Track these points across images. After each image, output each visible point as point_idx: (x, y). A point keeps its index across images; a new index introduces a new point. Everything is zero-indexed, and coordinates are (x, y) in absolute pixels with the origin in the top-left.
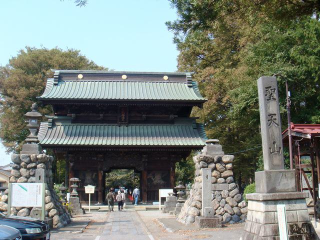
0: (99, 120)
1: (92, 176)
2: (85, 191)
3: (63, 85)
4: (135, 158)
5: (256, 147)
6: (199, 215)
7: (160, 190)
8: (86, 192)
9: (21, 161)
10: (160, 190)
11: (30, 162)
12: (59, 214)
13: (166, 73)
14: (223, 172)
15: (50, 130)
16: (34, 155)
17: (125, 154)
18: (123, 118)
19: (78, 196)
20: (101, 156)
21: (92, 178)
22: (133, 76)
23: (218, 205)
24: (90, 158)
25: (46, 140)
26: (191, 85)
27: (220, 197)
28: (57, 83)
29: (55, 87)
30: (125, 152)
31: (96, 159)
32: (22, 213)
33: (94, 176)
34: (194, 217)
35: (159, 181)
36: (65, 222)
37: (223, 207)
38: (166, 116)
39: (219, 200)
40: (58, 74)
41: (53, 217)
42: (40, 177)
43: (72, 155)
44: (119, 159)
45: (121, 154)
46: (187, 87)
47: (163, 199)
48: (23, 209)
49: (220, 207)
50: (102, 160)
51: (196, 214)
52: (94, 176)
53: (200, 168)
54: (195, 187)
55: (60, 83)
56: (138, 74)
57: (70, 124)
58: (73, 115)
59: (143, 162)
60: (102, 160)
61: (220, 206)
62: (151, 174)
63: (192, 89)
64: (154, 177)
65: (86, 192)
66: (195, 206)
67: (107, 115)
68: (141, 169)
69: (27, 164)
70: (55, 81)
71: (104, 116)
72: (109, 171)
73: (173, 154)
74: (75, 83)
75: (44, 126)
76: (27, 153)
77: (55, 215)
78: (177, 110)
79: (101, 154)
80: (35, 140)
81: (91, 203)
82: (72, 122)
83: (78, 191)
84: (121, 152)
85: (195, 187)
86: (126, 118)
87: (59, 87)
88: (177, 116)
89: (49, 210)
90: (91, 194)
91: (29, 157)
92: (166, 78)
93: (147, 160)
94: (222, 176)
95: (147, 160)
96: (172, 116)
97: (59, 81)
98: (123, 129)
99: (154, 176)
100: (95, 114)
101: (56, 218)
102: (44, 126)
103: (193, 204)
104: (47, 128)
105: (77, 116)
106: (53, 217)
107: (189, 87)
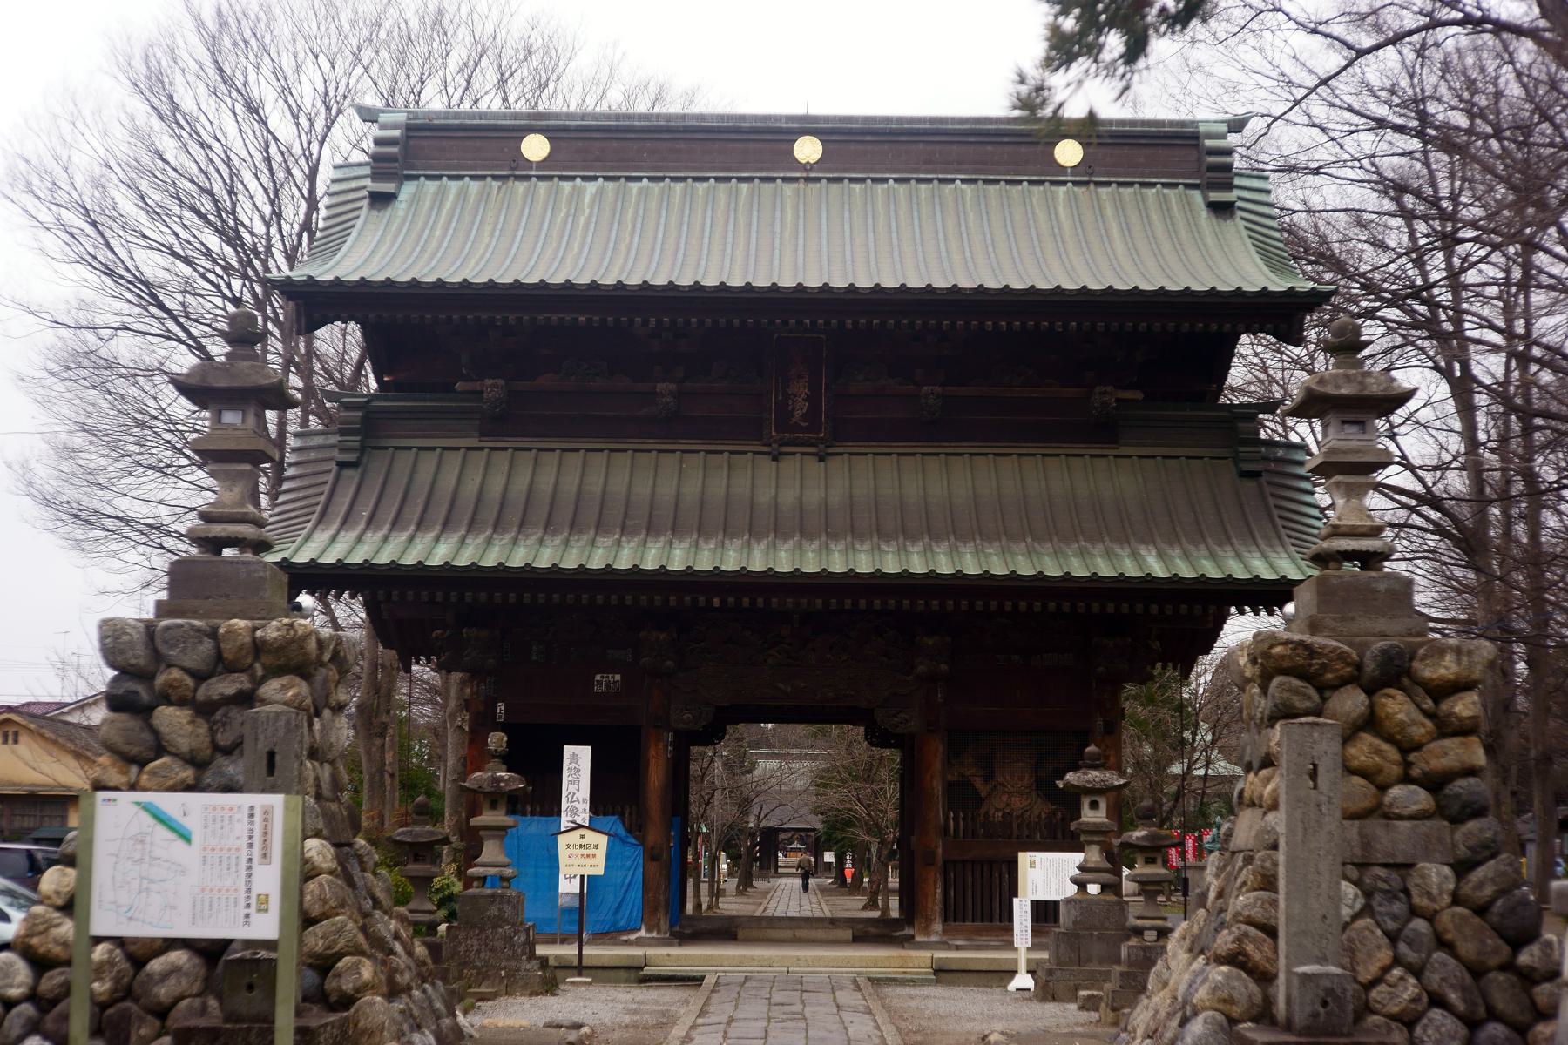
7: (1024, 858)
10: (1024, 858)
11: (222, 664)
18: (801, 407)
20: (662, 636)
40: (397, 133)
42: (271, 755)
57: (474, 442)
58: (493, 388)
69: (200, 677)
72: (712, 735)
82: (484, 434)
86: (814, 400)
95: (944, 667)
96: (1106, 396)
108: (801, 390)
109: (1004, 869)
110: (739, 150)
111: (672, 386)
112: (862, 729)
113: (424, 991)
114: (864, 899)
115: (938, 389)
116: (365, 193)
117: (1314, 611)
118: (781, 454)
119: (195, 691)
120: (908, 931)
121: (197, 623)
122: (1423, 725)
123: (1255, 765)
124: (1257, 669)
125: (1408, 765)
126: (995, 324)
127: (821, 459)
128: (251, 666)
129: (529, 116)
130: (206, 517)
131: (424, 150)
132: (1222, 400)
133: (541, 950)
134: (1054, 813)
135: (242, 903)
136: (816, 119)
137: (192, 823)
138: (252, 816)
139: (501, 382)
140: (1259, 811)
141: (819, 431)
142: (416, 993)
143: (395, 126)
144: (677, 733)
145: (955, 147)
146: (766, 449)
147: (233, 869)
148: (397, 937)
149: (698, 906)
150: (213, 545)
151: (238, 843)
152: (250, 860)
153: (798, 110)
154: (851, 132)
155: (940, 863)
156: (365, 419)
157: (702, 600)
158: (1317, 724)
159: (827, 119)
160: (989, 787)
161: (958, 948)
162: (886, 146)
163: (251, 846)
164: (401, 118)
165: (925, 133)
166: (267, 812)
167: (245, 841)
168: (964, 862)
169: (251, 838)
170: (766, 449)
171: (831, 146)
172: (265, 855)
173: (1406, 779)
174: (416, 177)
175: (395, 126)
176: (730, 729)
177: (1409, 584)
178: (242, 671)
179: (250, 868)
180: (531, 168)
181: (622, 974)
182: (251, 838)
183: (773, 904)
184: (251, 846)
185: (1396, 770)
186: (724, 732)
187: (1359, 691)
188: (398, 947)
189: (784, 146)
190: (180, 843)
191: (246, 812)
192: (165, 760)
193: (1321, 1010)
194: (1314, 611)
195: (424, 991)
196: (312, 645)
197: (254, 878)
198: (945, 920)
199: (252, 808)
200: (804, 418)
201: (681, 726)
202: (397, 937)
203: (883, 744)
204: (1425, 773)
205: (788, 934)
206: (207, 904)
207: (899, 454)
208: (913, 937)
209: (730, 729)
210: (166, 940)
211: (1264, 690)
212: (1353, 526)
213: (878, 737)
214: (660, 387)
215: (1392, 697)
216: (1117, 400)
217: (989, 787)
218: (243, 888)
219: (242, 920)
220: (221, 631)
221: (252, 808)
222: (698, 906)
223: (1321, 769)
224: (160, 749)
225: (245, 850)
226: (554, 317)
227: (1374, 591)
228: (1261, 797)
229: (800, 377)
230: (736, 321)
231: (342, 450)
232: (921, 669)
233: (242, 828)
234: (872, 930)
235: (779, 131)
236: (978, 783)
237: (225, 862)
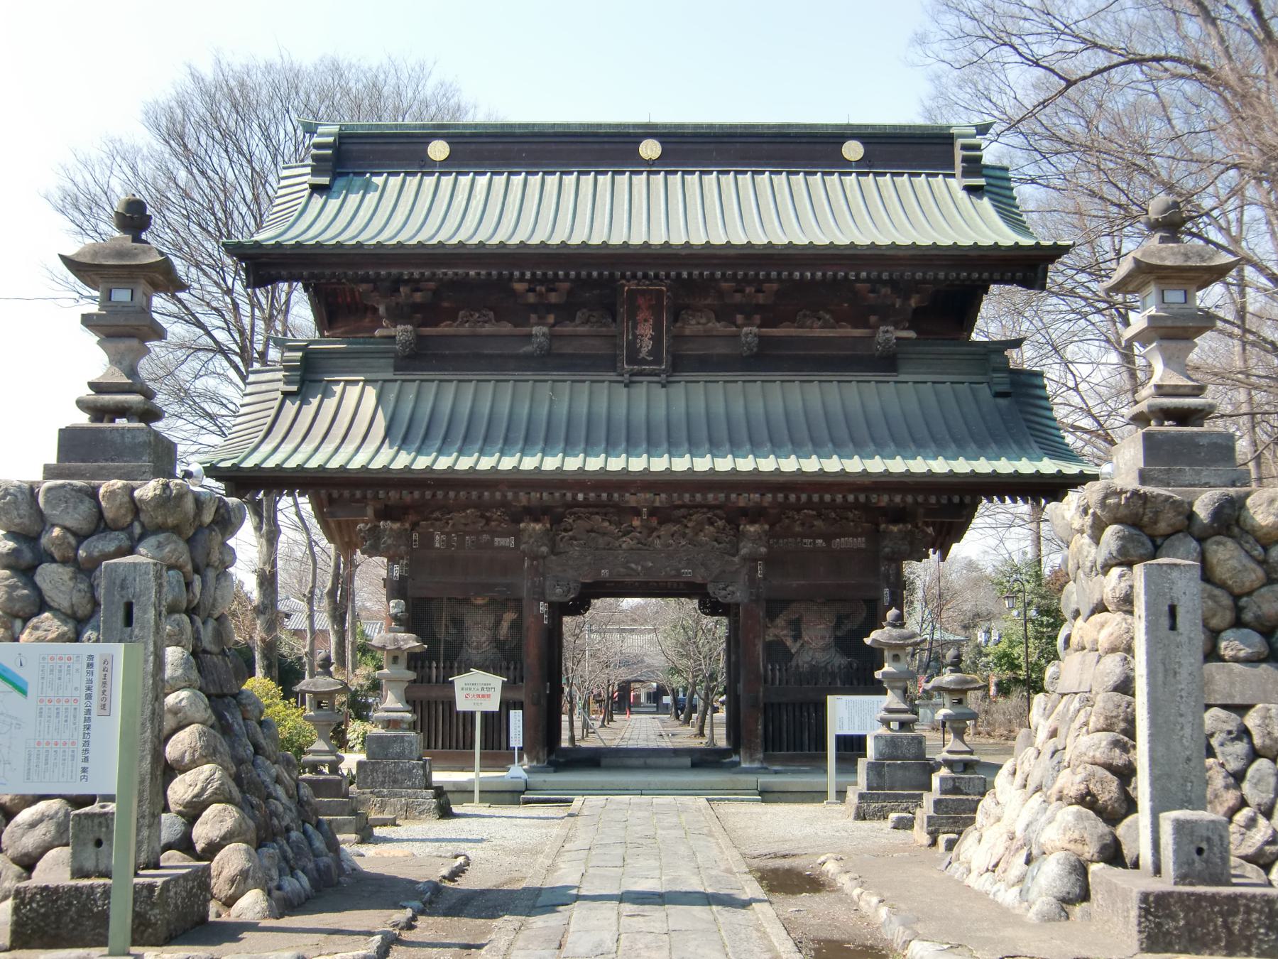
0: (528, 357)
1: (498, 623)
2: (452, 703)
3: (354, 199)
4: (702, 538)
5: (181, 881)
6: (1113, 855)
7: (829, 697)
8: (462, 705)
9: (43, 521)
10: (829, 697)
11: (100, 525)
12: (262, 834)
13: (849, 126)
14: (1249, 594)
15: (291, 408)
16: (118, 483)
17: (654, 522)
18: (646, 346)
19: (413, 726)
20: (538, 527)
21: (494, 639)
22: (696, 148)
23: (1230, 798)
24: (485, 537)
25: (266, 448)
26: (981, 182)
27: (1241, 747)
28: (325, 180)
29: (318, 201)
30: (653, 512)
31: (511, 542)
32: (33, 825)
33: (505, 626)
34: (1080, 870)
35: (822, 657)
36: (299, 883)
37: (1268, 814)
38: (858, 332)
39: (1233, 765)
40: (331, 139)
41: (212, 849)
42: (129, 607)
43: (396, 526)
44: (627, 542)
45: (636, 523)
46: (962, 195)
47: (852, 746)
48: (42, 806)
49: (1246, 812)
50: (544, 549)
51: (1090, 850)
52: (505, 626)
53: (1106, 568)
54: (1066, 683)
55: (341, 182)
56: (715, 135)
57: (390, 376)
58: (402, 331)
59: (744, 559)
60: (544, 549)
61: (1243, 803)
62: (780, 621)
63: (986, 202)
64: (797, 637)
65: (462, 705)
66: (1087, 800)
67: (568, 329)
68: (738, 593)
69: (81, 537)
70: (315, 172)
71: (552, 337)
72: (579, 606)
73: (895, 521)
74: (413, 182)
75: (264, 387)
76: (81, 476)
77: (227, 839)
78: (913, 303)
79: (537, 520)
80: (135, 398)
81: (483, 757)
82: (397, 369)
83: (412, 702)
84: (636, 512)
85: (1066, 683)
86: (657, 340)
87: (334, 204)
88: (912, 334)
89: (192, 812)
90: (485, 715)
91: (93, 493)
92: (853, 150)
93: (763, 550)
94: (1248, 616)
95: (763, 550)
96: (889, 334)
97: (335, 176)
98: (649, 400)
99: (796, 628)
100: (506, 328)
101: (232, 859)
102: (264, 387)
103: (1071, 782)
104: (280, 397)
105: (420, 338)
106: (212, 849)
107: (970, 190)
108: (646, 330)
109: (812, 709)
110: (600, 149)
111: (545, 329)
112: (696, 601)
113: (305, 832)
114: (695, 730)
115: (755, 329)
116: (306, 186)
117: (1141, 465)
118: (632, 382)
119: (77, 549)
120: (735, 758)
121: (78, 483)
122: (1254, 571)
123: (1085, 611)
124: (1088, 520)
125: (1238, 610)
126: (801, 275)
127: (664, 386)
128: (131, 524)
129: (435, 127)
130: (97, 387)
131: (351, 157)
132: (975, 337)
133: (438, 777)
134: (850, 664)
135: (80, 756)
136: (655, 126)
137: (28, 675)
138: (90, 665)
139: (409, 327)
140: (1094, 655)
141: (661, 364)
142: (295, 835)
143: (329, 135)
144: (551, 605)
145: (765, 146)
146: (620, 378)
147: (71, 719)
148: (278, 780)
149: (572, 738)
150: (98, 412)
151: (76, 694)
152: (88, 712)
153: (643, 119)
154: (683, 135)
155: (762, 705)
156: (304, 359)
157: (569, 495)
158: (1175, 565)
159: (665, 126)
160: (798, 645)
161: (776, 772)
162: (712, 146)
163: (89, 697)
164: (335, 129)
165: (741, 135)
166: (107, 664)
167: (84, 692)
168: (780, 704)
169: (89, 688)
170: (620, 378)
171: (669, 146)
172: (103, 707)
173: (1238, 623)
174: (347, 174)
175: (329, 135)
176: (594, 601)
177: (1231, 438)
178: (122, 529)
179: (87, 720)
180: (435, 166)
181: (507, 796)
182: (89, 688)
183: (304, 323)
184: (89, 697)
185: (1229, 616)
186: (589, 604)
187: (1190, 539)
188: (280, 791)
189: (632, 146)
190: (16, 695)
191: (85, 661)
192: (47, 614)
193: (1196, 857)
194: (1141, 465)
195: (305, 832)
196: (189, 504)
197: (92, 731)
198: (766, 750)
199: (91, 657)
200: (649, 353)
201: (554, 599)
202: (278, 780)
203: (713, 612)
204: (1257, 617)
205: (640, 762)
206: (43, 758)
207: (725, 382)
208: (739, 763)
209: (594, 601)
210: (34, 796)
211: (1096, 539)
212: (1176, 386)
213: (711, 607)
214: (535, 330)
215: (1224, 544)
216: (897, 338)
217: (798, 645)
218: (81, 741)
219: (80, 774)
220: (102, 491)
221: (91, 657)
222: (572, 738)
223: (1181, 612)
224: (42, 605)
225: (83, 700)
226: (450, 272)
227: (1198, 445)
228: (1096, 642)
229: (646, 321)
230: (595, 274)
231: (286, 383)
232: (744, 551)
233: (80, 680)
234: (710, 758)
235: (628, 135)
236: (789, 642)
237: (62, 711)
